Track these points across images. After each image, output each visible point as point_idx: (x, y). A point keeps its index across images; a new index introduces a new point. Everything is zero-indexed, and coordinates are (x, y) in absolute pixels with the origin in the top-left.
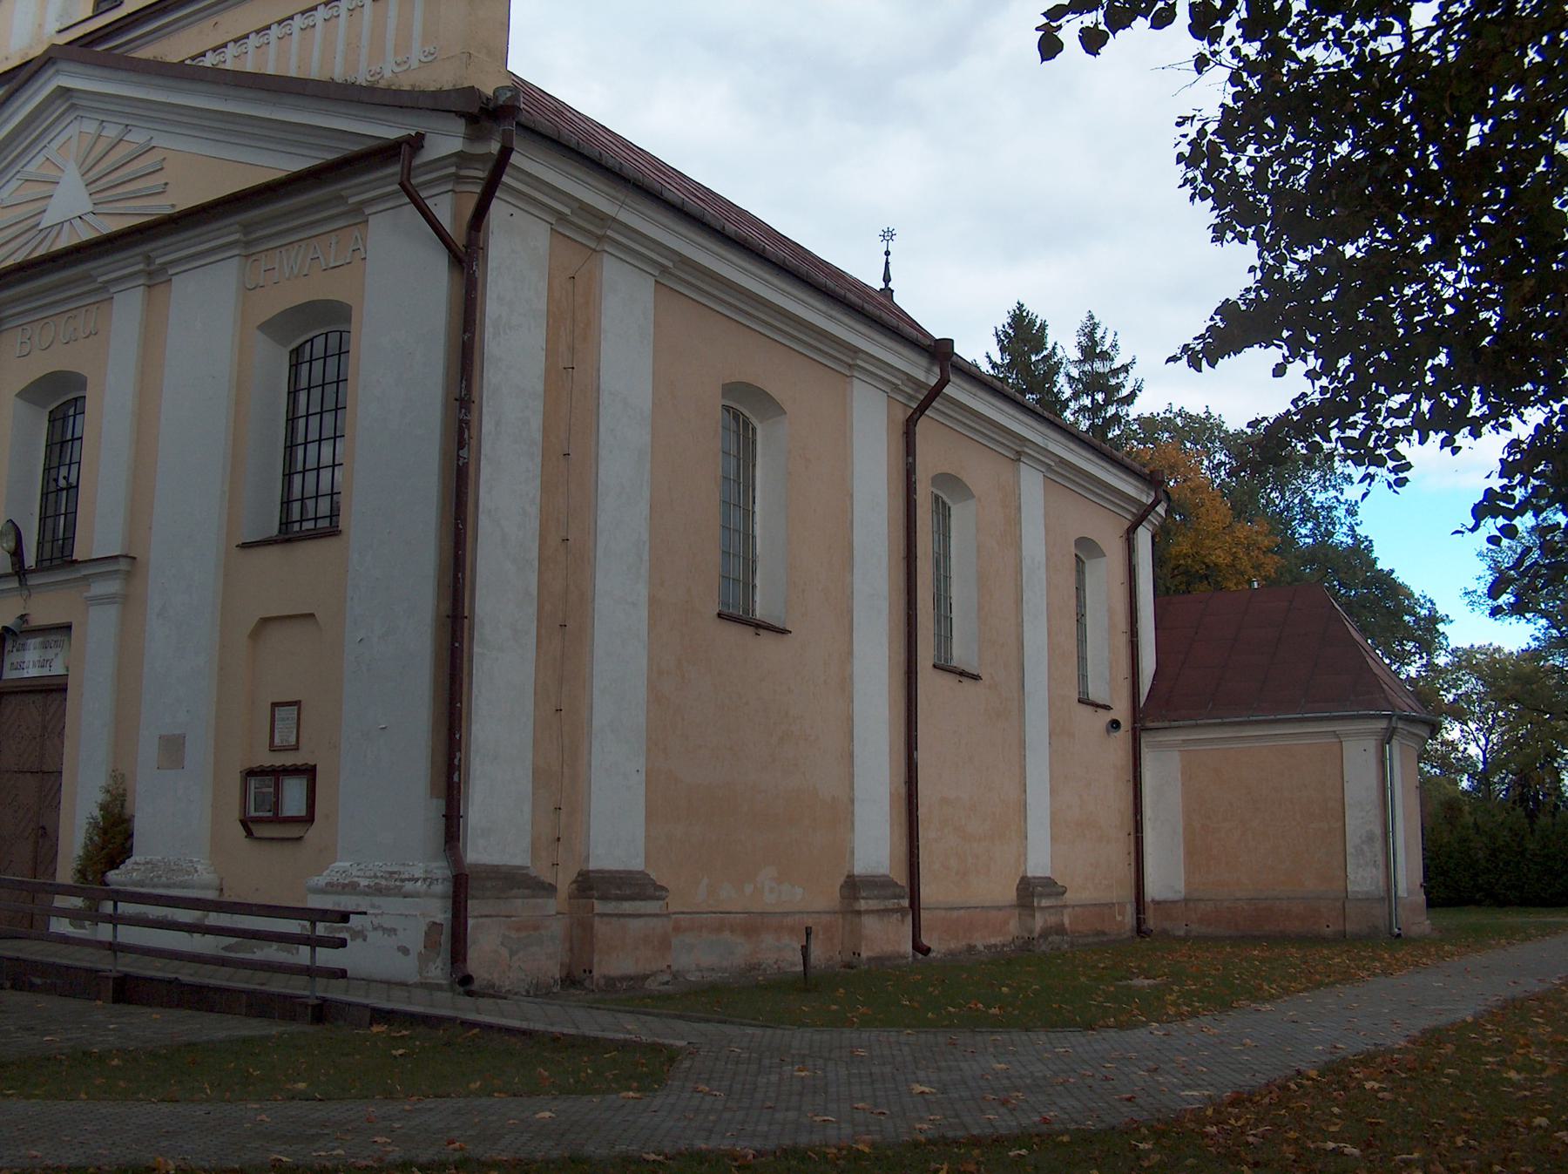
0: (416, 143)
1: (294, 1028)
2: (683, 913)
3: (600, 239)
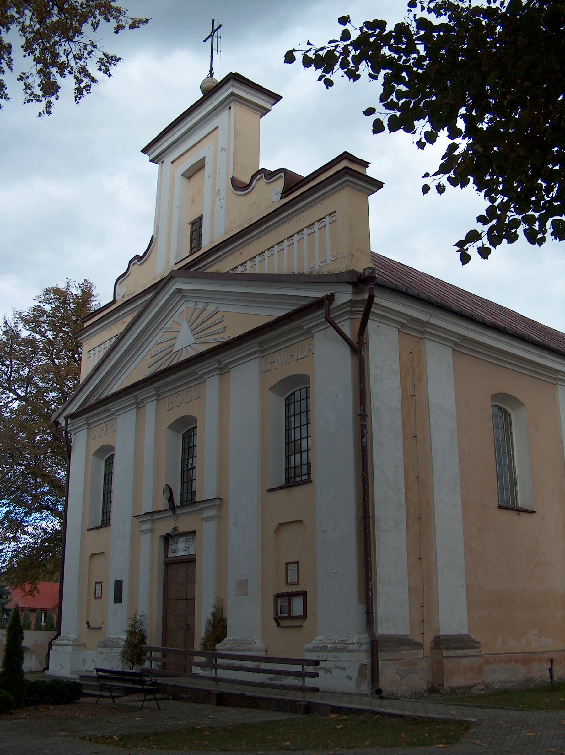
0: (331, 298)
1: (293, 716)
2: (490, 654)
3: (422, 332)
